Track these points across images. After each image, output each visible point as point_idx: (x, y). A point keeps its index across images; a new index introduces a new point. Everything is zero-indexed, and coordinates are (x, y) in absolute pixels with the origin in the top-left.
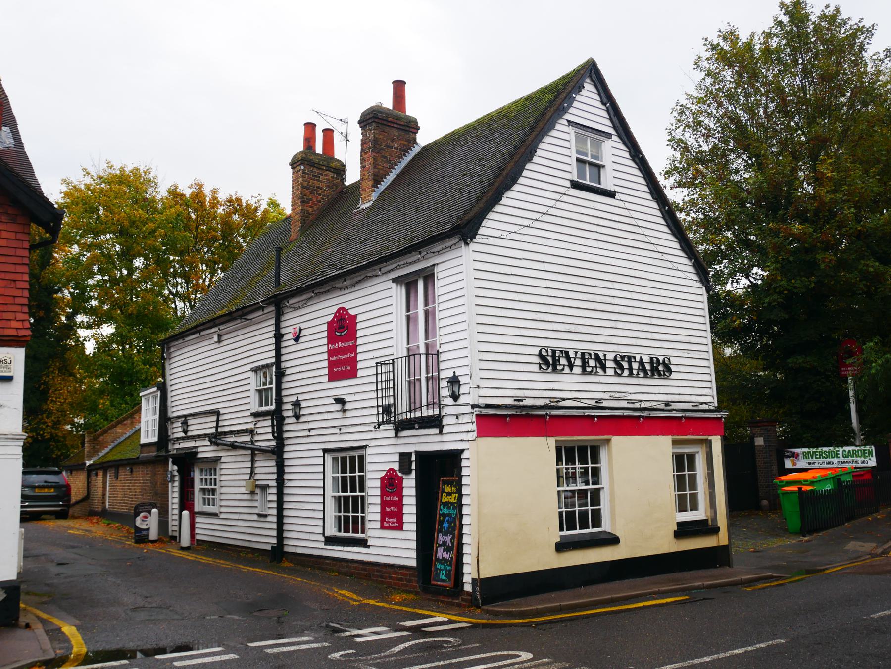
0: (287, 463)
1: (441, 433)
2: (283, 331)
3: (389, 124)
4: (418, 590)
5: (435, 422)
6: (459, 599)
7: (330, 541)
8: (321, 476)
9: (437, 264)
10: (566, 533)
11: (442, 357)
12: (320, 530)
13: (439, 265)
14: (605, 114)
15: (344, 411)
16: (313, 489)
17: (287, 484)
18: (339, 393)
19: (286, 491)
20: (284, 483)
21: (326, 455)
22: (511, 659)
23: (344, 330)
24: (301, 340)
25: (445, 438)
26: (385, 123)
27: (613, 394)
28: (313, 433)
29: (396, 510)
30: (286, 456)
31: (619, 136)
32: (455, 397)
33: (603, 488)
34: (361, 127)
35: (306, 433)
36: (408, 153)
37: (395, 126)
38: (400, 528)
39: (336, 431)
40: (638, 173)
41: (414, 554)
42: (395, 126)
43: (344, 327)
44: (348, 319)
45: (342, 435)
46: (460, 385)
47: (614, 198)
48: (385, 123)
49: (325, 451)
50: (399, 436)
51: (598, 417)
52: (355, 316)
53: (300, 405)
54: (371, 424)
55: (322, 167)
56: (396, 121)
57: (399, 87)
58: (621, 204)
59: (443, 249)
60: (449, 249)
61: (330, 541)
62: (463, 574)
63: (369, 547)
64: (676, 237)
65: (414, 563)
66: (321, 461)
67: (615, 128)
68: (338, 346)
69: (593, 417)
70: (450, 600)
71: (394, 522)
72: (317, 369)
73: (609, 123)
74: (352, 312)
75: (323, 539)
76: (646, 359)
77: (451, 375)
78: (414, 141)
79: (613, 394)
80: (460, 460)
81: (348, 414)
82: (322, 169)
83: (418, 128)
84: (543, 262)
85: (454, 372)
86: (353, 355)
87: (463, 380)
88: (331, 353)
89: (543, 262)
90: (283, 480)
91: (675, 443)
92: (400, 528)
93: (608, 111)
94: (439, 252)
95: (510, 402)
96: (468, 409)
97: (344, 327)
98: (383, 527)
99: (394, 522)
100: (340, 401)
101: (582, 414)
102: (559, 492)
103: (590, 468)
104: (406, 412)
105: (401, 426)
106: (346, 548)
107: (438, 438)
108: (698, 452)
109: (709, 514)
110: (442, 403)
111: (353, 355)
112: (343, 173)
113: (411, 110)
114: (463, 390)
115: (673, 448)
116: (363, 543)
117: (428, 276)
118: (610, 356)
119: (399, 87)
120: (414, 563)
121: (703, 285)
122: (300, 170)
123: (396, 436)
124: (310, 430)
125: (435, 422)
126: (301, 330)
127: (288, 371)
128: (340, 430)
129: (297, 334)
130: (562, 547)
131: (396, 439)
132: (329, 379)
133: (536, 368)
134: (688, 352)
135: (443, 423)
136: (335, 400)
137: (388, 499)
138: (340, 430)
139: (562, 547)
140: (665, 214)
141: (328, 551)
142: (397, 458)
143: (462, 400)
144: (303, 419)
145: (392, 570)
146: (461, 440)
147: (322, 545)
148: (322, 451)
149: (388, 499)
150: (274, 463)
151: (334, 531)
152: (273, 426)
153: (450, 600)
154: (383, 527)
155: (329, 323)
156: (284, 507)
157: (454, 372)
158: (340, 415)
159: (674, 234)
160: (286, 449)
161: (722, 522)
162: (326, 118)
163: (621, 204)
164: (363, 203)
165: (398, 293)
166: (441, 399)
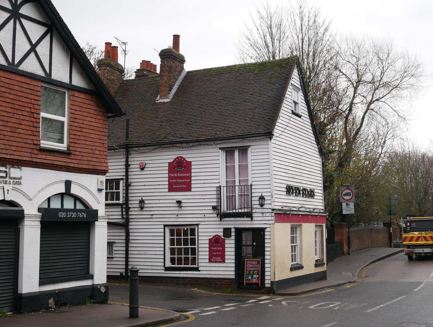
0: (130, 231)
1: (252, 220)
2: (130, 163)
3: (176, 59)
4: (235, 288)
5: (249, 215)
6: (262, 290)
7: (167, 269)
8: (163, 238)
9: (251, 145)
10: (294, 263)
11: (253, 187)
12: (162, 264)
13: (252, 146)
14: (299, 80)
15: (181, 207)
16: (153, 244)
17: (131, 241)
18: (179, 198)
19: (130, 245)
20: (129, 241)
21: (166, 228)
22: (332, 304)
23: (182, 167)
24: (145, 169)
25: (254, 222)
26: (175, 58)
27: (303, 205)
28: (154, 216)
29: (220, 253)
30: (130, 227)
31: (302, 90)
32: (262, 205)
33: (297, 245)
34: (160, 57)
35: (150, 217)
36: (181, 74)
37: (178, 60)
38: (223, 261)
39: (175, 216)
40: (305, 106)
41: (233, 273)
42: (178, 60)
43: (182, 166)
44: (185, 163)
45: (206, 218)
46: (265, 200)
47: (301, 118)
48: (175, 58)
49: (165, 226)
50: (222, 220)
51: (301, 215)
52: (191, 162)
53: (144, 202)
54: (202, 214)
55: (115, 69)
56: (178, 57)
57: (176, 38)
58: (302, 121)
59: (258, 139)
60: (260, 140)
61: (167, 269)
62: (265, 279)
63: (200, 271)
64: (314, 135)
65: (233, 277)
66: (163, 230)
67: (301, 86)
68: (177, 175)
69: (300, 214)
70: (257, 291)
71: (219, 259)
72: (159, 185)
73: (299, 83)
74: (188, 160)
75: (164, 269)
76: (309, 189)
77: (260, 195)
78: (182, 68)
79: (303, 205)
80: (264, 232)
81: (183, 208)
82: (115, 70)
83: (185, 61)
84: (286, 147)
85: (262, 194)
86: (189, 180)
87: (266, 198)
88: (170, 178)
89: (286, 147)
90: (129, 239)
91: (316, 226)
92: (223, 261)
93: (300, 78)
94: (253, 140)
95: (280, 208)
96: (270, 211)
97: (182, 166)
98: (210, 261)
99: (219, 259)
100: (179, 202)
101: (297, 213)
102: (292, 246)
103: (188, 237)
104: (238, 209)
105: (222, 216)
106: (181, 272)
107: (250, 222)
108: (317, 230)
109: (321, 257)
110: (253, 207)
111: (189, 180)
112: (123, 72)
113: (182, 51)
114: (266, 202)
115: (315, 228)
116: (197, 269)
117: (244, 151)
118: (301, 188)
119: (176, 38)
120: (233, 277)
121: (321, 157)
122: (106, 69)
123: (221, 220)
124: (152, 215)
125: (249, 215)
126: (146, 164)
127: (133, 184)
128: (204, 215)
129: (144, 166)
130: (292, 269)
131: (220, 222)
132: (168, 191)
133: (285, 193)
134: (318, 187)
135: (253, 216)
136: (176, 201)
137: (220, 248)
138: (177, 216)
139: (292, 269)
140: (313, 126)
141: (167, 274)
142: (222, 230)
143: (265, 206)
144: (145, 209)
145: (217, 281)
146: (265, 224)
147: (163, 271)
148: (163, 225)
149: (220, 248)
150: (124, 231)
151: (170, 265)
152: (122, 211)
153: (257, 291)
154: (210, 261)
155: (169, 163)
156: (129, 253)
157: (262, 194)
158: (178, 209)
159: (314, 134)
160: (130, 224)
161: (325, 261)
162: (118, 40)
163: (302, 121)
164: (161, 98)
165: (222, 155)
166: (253, 205)
